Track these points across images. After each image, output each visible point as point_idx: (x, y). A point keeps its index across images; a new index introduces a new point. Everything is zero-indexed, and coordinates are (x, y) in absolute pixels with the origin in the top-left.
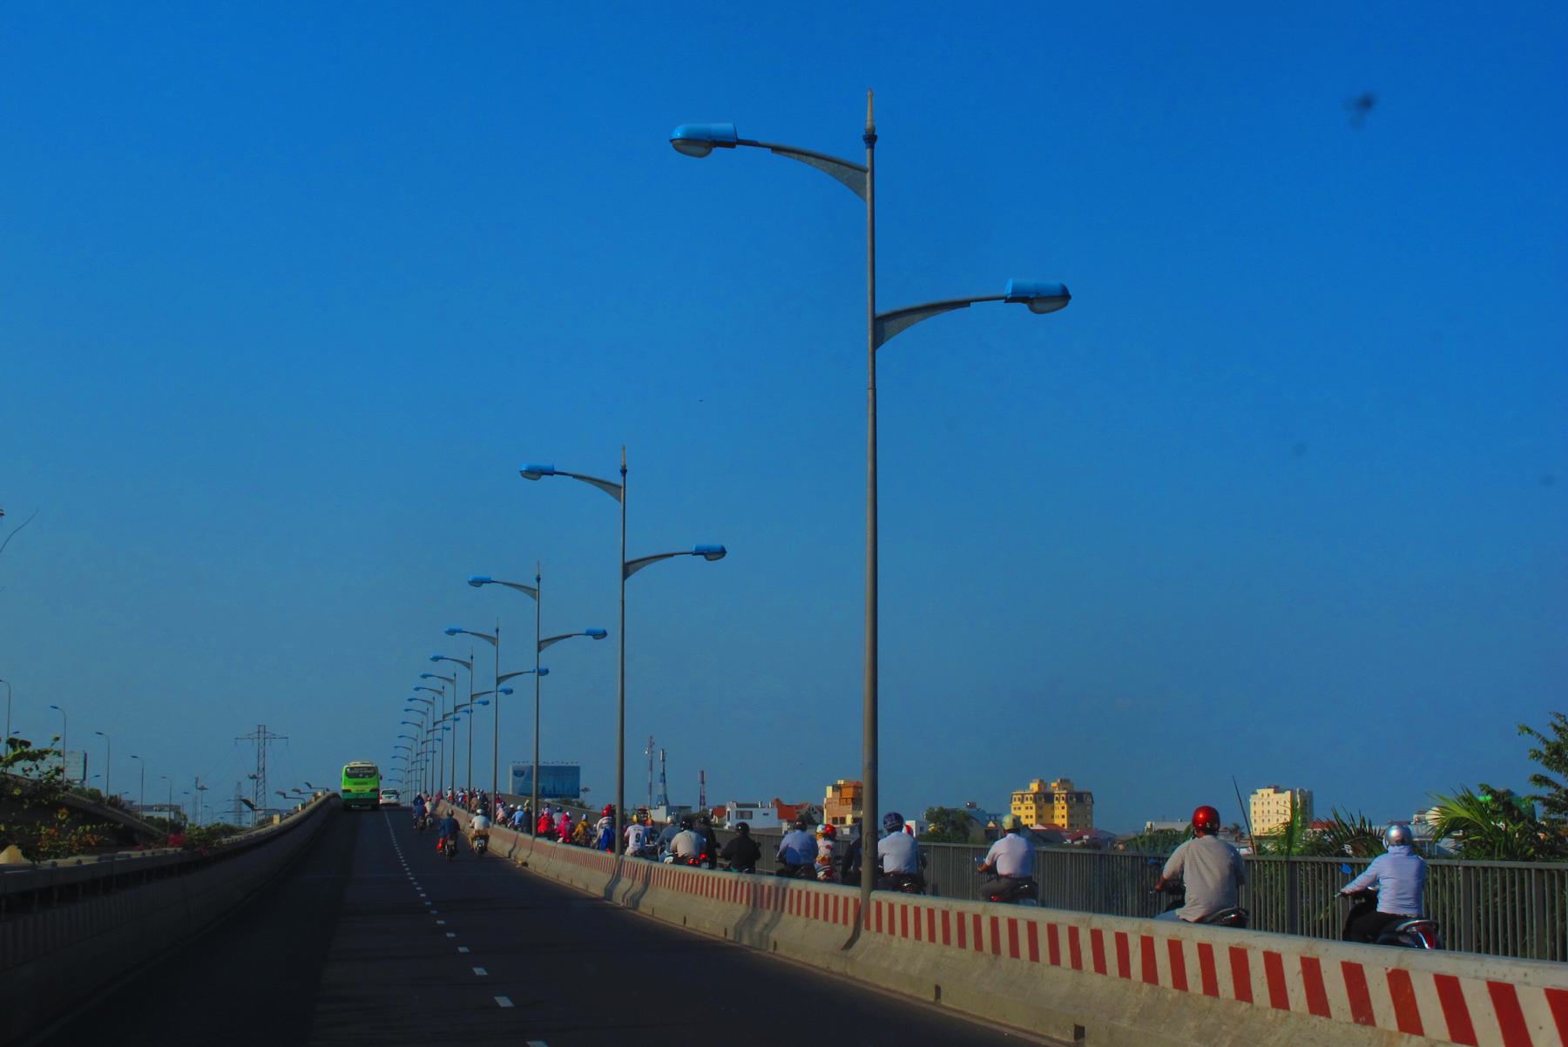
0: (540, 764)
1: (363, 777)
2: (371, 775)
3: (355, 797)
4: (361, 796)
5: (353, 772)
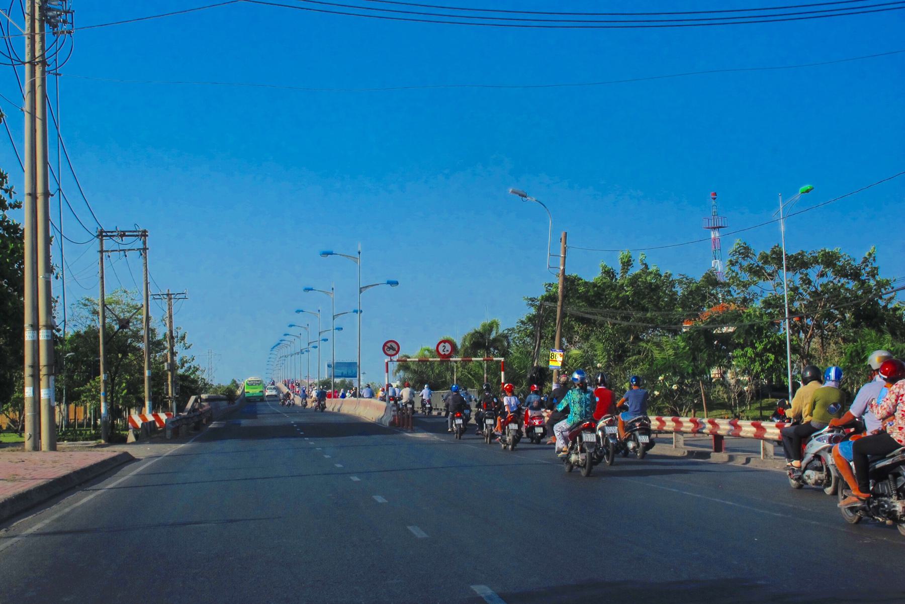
0: (566, 274)
1: (256, 385)
2: (259, 384)
3: (251, 395)
4: (255, 395)
5: (250, 383)
